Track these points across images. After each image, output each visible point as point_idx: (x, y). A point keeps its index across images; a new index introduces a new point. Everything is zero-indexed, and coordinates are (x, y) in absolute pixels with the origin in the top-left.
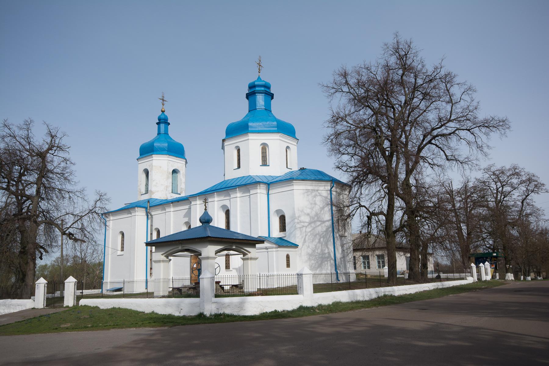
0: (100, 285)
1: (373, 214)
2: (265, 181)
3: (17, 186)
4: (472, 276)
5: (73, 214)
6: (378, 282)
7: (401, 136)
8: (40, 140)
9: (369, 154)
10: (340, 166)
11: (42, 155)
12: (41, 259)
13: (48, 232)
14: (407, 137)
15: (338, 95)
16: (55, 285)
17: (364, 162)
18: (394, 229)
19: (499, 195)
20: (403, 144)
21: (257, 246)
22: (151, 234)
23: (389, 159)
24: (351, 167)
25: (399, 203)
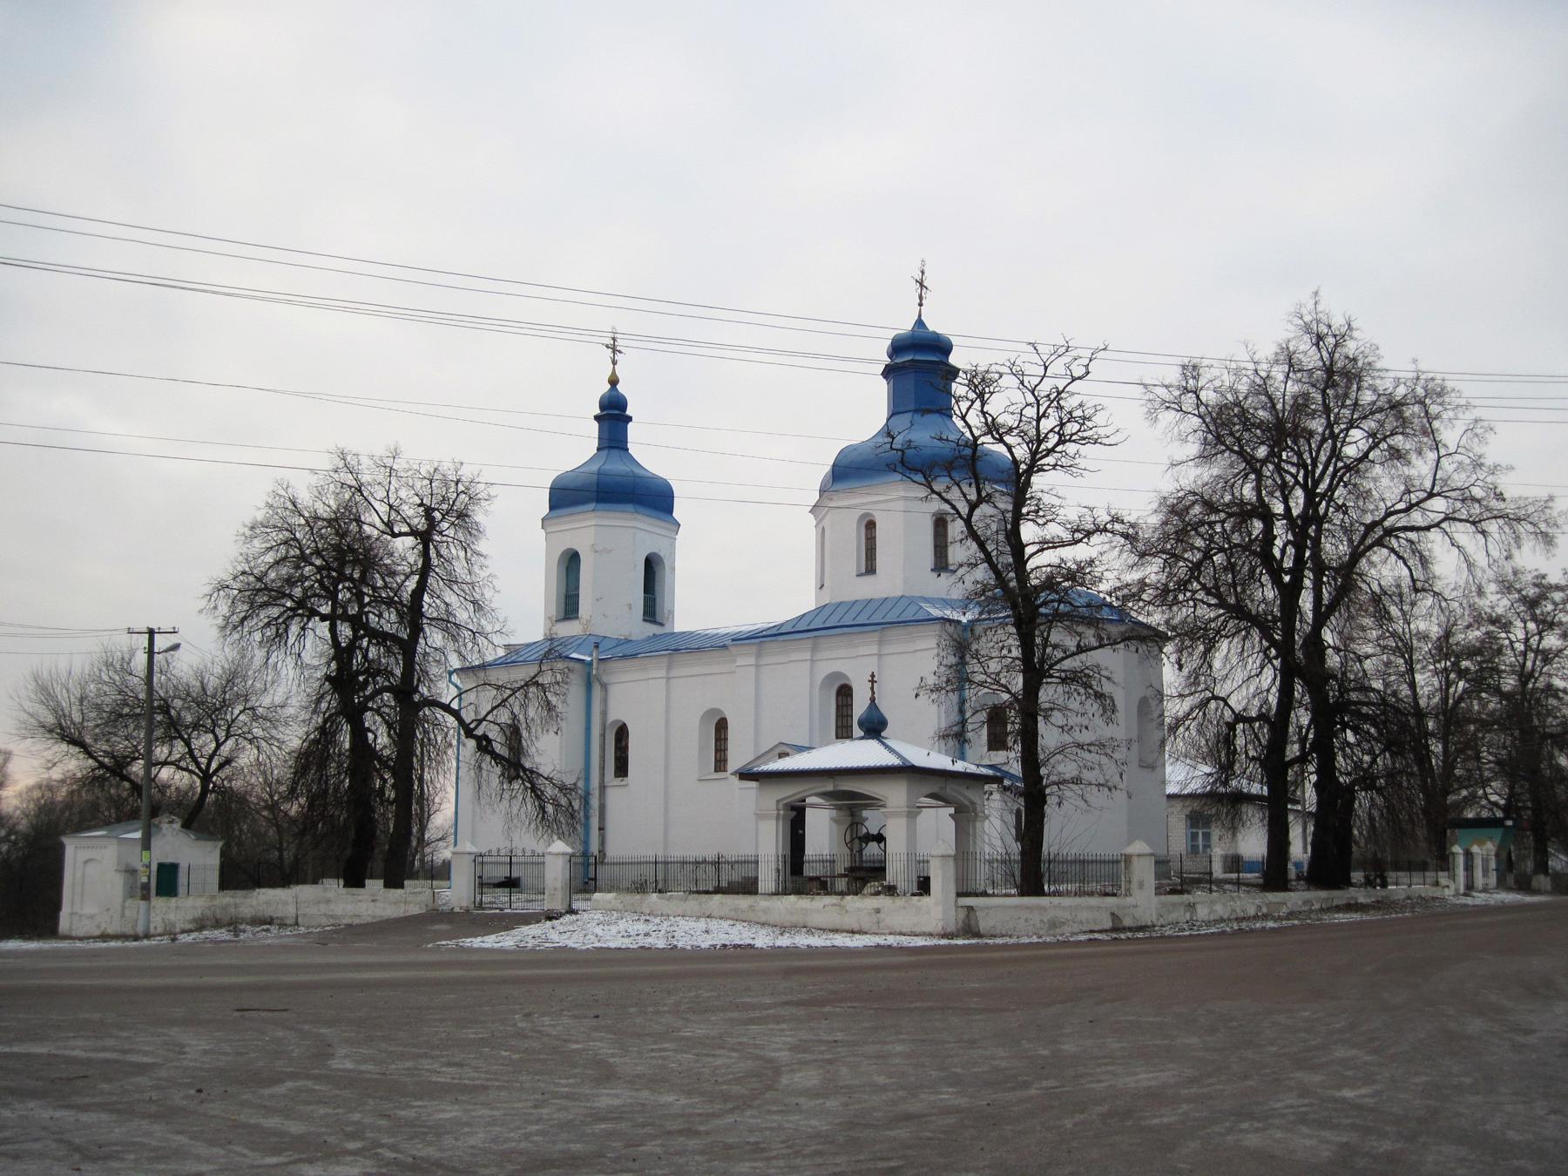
4: (1453, 877)
19: (1531, 656)
23: (1290, 594)
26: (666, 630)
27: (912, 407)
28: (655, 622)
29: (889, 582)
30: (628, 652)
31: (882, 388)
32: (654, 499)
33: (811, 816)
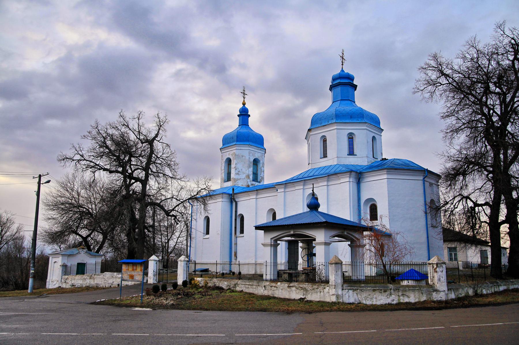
28: (257, 182)
29: (331, 161)
30: (247, 191)
32: (258, 141)
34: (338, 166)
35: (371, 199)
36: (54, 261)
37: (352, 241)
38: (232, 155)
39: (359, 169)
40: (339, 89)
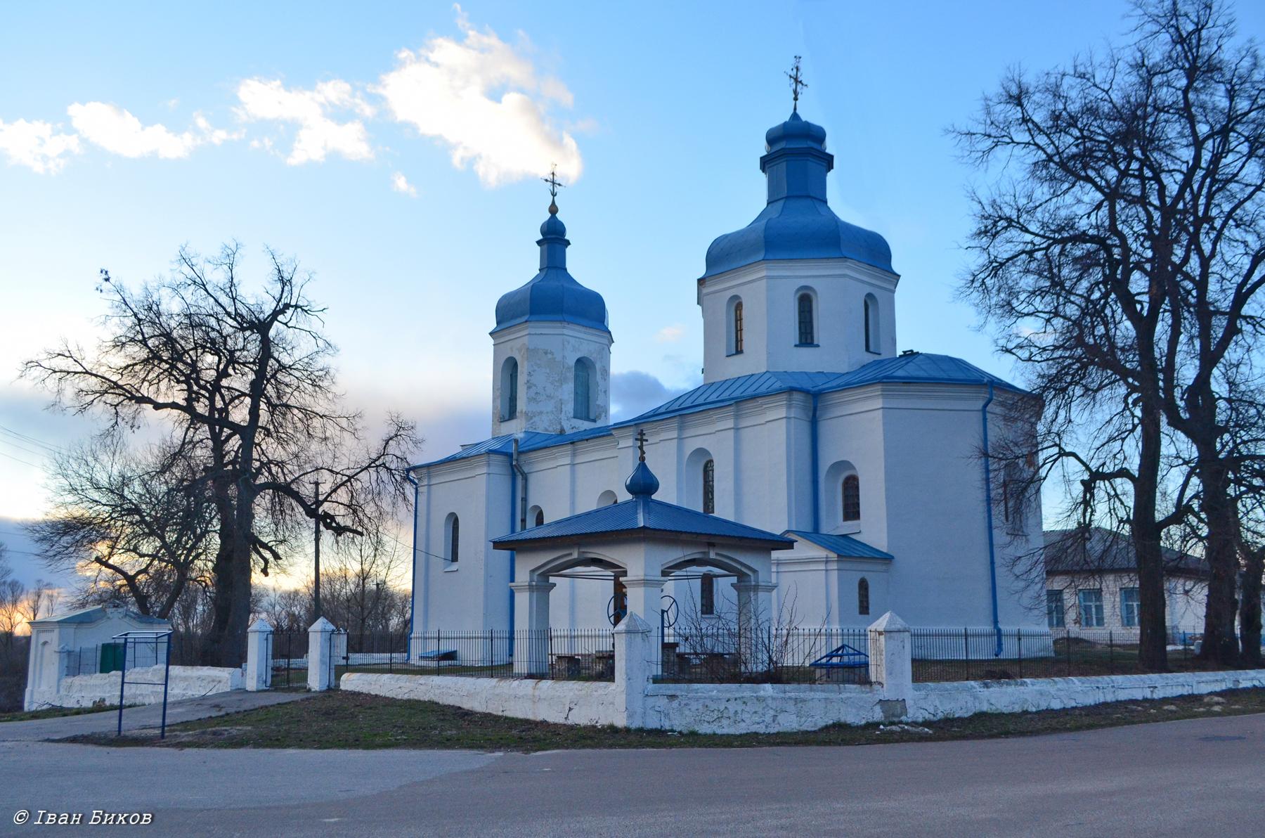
0: (400, 642)
1: (1096, 476)
2: (808, 385)
3: (212, 400)
5: (331, 471)
6: (1110, 661)
7: (1186, 260)
8: (257, 293)
9: (1093, 311)
10: (1011, 346)
11: (262, 327)
12: (266, 574)
13: (277, 512)
14: (1205, 263)
15: (1002, 153)
16: (289, 641)
17: (1076, 335)
18: (1159, 517)
20: (1192, 279)
21: (775, 555)
22: (524, 521)
23: (1145, 326)
24: (1044, 349)
25: (1176, 445)
26: (599, 424)
27: (785, 194)
28: (588, 418)
29: (753, 362)
31: (762, 180)
32: (589, 311)
33: (517, 596)
34: (768, 375)
35: (844, 465)
36: (42, 641)
37: (741, 576)
38: (520, 350)
39: (820, 384)
40: (782, 167)
